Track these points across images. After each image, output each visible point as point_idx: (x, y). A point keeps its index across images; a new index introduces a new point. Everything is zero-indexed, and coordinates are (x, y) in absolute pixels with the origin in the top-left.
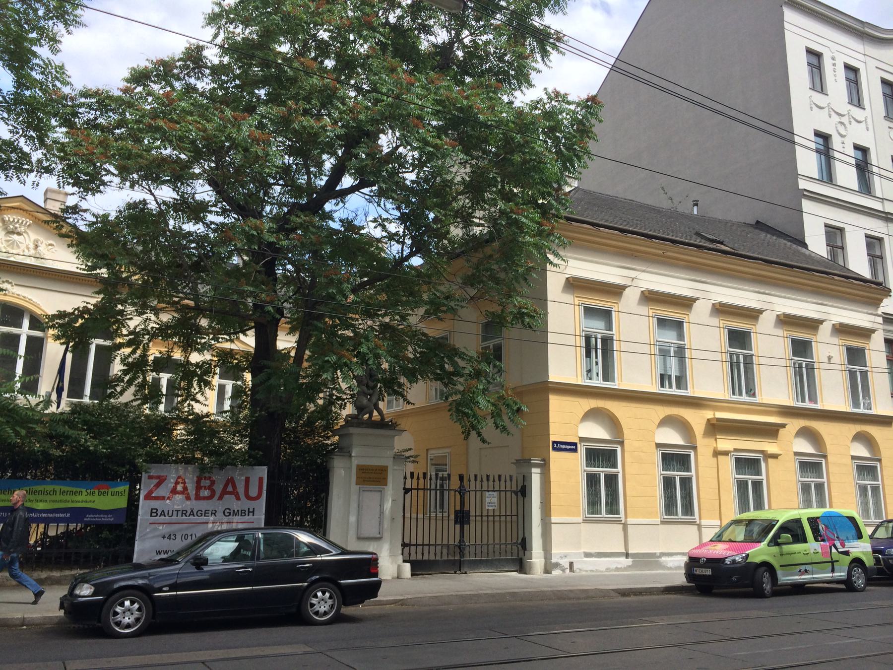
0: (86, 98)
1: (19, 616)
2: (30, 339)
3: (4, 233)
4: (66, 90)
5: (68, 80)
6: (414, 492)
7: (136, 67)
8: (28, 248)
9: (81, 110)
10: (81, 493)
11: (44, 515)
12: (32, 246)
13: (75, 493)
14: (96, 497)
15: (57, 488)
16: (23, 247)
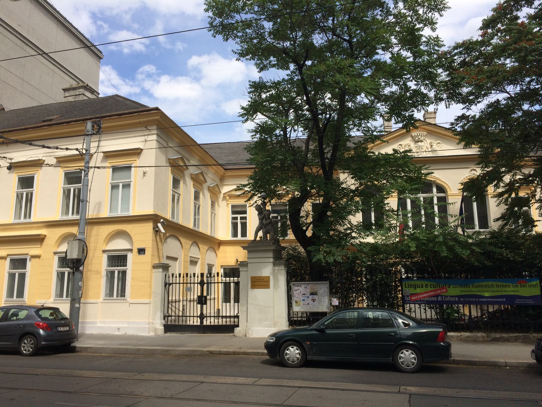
0: (457, 49)
1: (218, 350)
2: (439, 199)
3: (413, 143)
4: (444, 49)
5: (442, 43)
6: (174, 285)
7: (486, 18)
8: (427, 148)
9: (455, 58)
10: (509, 286)
11: (489, 300)
12: (429, 146)
13: (506, 286)
14: (519, 288)
15: (494, 283)
16: (425, 148)
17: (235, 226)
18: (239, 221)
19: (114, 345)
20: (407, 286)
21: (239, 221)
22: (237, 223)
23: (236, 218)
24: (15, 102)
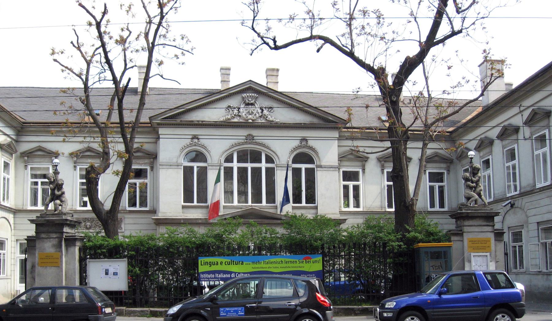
2: (267, 169)
14: (304, 264)
17: (346, 196)
18: (40, 187)
19: (277, 307)
20: (203, 264)
21: (40, 187)
22: (37, 189)
23: (36, 183)
24: (551, 88)
